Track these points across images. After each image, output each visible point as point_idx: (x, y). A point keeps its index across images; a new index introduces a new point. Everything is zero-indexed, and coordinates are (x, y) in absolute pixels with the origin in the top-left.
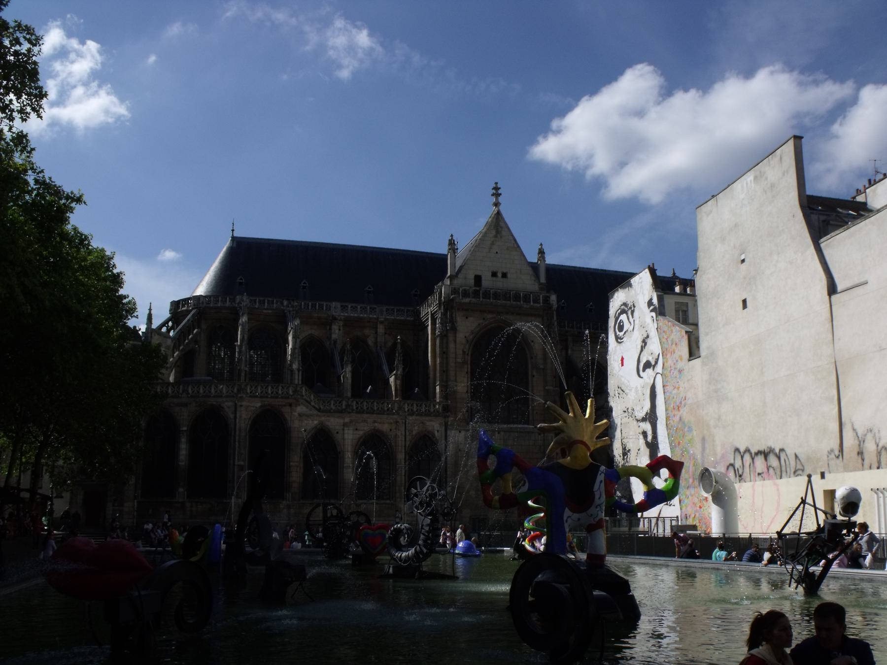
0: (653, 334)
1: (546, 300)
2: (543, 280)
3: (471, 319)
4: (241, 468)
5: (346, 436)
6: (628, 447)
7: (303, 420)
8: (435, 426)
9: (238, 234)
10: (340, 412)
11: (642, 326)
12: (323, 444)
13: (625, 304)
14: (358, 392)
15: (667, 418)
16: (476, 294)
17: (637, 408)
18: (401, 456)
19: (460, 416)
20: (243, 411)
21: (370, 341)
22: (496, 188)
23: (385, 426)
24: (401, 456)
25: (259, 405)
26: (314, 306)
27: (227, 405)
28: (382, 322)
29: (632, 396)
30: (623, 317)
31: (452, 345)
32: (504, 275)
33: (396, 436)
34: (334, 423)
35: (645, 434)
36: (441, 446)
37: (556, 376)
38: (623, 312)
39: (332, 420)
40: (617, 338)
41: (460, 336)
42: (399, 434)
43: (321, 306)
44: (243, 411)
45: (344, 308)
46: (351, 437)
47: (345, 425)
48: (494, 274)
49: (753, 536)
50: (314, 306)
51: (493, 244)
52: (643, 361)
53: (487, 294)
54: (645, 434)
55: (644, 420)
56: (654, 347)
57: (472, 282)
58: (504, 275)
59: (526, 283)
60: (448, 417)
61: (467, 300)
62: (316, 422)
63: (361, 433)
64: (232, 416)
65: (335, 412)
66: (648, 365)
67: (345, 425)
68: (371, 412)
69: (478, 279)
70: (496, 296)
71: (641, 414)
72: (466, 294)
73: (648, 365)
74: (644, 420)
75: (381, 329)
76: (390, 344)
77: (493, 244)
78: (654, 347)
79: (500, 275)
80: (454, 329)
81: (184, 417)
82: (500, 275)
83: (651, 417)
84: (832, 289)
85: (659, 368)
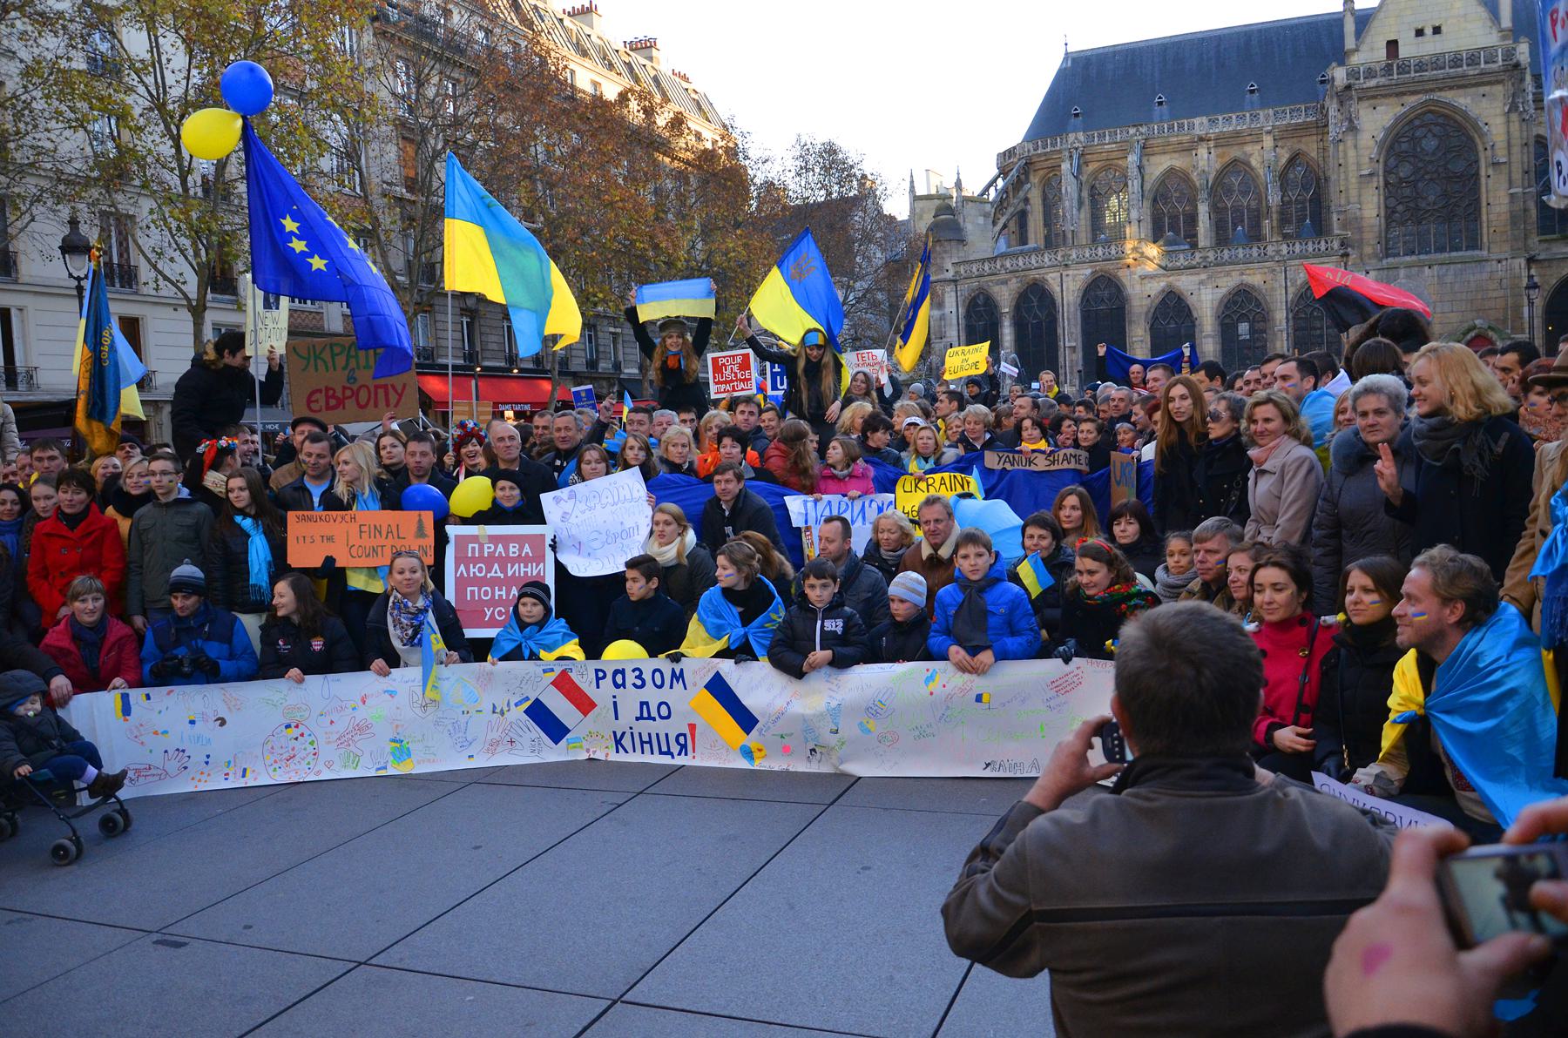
1: (1509, 54)
2: (1506, 22)
4: (1073, 349)
5: (1203, 297)
9: (1074, 47)
11: (1026, 200)
12: (1173, 314)
16: (1388, 69)
18: (1280, 316)
19: (1368, 250)
20: (1067, 287)
23: (1255, 278)
24: (1280, 316)
25: (1089, 271)
26: (1171, 128)
28: (1269, 132)
31: (1351, 153)
32: (1437, 30)
33: (1273, 289)
34: (1185, 283)
37: (164, 775)
39: (1183, 278)
42: (1276, 285)
43: (1181, 126)
44: (1067, 287)
45: (1213, 122)
46: (1210, 297)
47: (1201, 283)
48: (1420, 33)
50: (1171, 128)
53: (1404, 68)
57: (1382, 54)
58: (1437, 30)
61: (1373, 83)
62: (1163, 284)
63: (1224, 290)
64: (1058, 289)
65: (1186, 268)
68: (1233, 262)
69: (1392, 46)
70: (1421, 67)
72: (1370, 74)
75: (1268, 141)
79: (1428, 31)
80: (1353, 129)
81: (1005, 297)
82: (1428, 31)
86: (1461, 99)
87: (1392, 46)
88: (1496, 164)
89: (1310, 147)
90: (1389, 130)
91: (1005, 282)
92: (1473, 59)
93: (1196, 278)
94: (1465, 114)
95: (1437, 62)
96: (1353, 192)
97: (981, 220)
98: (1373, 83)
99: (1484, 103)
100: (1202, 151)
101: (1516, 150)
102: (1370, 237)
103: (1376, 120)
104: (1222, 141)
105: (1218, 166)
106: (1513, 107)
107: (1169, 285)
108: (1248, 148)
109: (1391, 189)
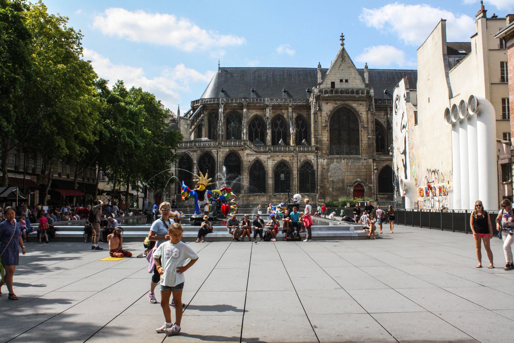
2: (367, 82)
7: (248, 157)
8: (311, 157)
10: (265, 152)
12: (258, 167)
19: (324, 152)
22: (342, 36)
31: (320, 118)
32: (347, 81)
36: (315, 168)
41: (324, 114)
43: (261, 100)
48: (341, 81)
51: (340, 65)
53: (337, 92)
54: (403, 160)
55: (403, 154)
61: (327, 95)
63: (276, 162)
64: (216, 156)
66: (404, 127)
69: (333, 84)
70: (342, 92)
72: (326, 92)
74: (403, 154)
75: (290, 110)
77: (340, 65)
79: (344, 81)
80: (320, 110)
82: (344, 81)
83: (404, 153)
86: (354, 105)
87: (333, 84)
88: (364, 127)
89: (304, 114)
90: (331, 112)
91: (195, 151)
92: (357, 92)
93: (266, 156)
94: (355, 109)
95: (347, 91)
96: (320, 131)
97: (186, 126)
98: (327, 95)
99: (361, 107)
100: (268, 110)
101: (370, 123)
102: (325, 147)
103: (328, 108)
104: (274, 108)
105: (273, 116)
106: (369, 110)
107: (257, 158)
108: (283, 111)
109: (332, 132)
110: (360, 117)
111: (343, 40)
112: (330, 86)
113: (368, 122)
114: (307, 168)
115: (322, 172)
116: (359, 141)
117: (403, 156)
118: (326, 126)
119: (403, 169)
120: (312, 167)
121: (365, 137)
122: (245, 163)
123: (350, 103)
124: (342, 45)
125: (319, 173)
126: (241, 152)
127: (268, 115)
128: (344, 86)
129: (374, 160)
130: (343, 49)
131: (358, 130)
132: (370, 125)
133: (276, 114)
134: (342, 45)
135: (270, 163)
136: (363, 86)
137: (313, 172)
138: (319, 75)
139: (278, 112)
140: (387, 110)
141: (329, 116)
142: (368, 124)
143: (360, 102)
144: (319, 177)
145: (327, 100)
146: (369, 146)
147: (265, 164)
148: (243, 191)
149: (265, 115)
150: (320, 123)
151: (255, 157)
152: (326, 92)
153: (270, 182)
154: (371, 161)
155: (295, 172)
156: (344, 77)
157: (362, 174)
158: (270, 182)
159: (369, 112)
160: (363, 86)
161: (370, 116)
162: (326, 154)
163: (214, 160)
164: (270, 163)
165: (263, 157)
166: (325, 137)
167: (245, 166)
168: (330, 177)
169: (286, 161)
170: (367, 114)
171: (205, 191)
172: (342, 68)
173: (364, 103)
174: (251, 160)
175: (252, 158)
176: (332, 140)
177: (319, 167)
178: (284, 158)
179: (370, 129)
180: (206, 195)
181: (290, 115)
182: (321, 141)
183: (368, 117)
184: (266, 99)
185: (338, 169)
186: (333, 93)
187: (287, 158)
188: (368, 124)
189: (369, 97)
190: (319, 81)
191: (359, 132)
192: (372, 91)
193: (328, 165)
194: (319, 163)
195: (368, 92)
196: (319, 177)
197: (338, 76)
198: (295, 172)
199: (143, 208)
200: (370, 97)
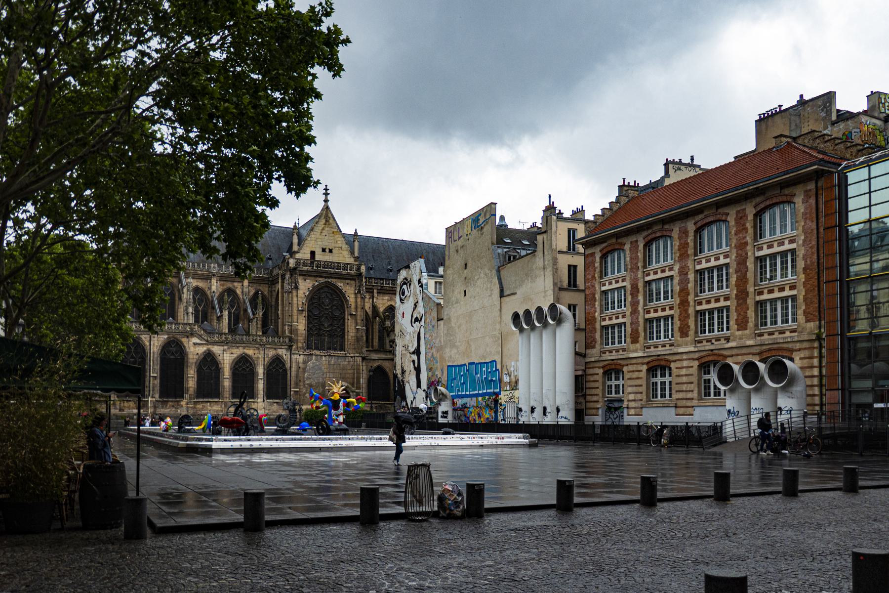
0: (420, 301)
3: (308, 281)
6: (405, 368)
7: (195, 348)
8: (283, 352)
12: (209, 362)
13: (406, 279)
14: (232, 330)
15: (426, 354)
17: (410, 345)
19: (300, 345)
21: (239, 291)
27: (145, 338)
29: (408, 337)
30: (405, 287)
31: (295, 299)
32: (331, 251)
35: (414, 362)
36: (288, 366)
38: (405, 283)
40: (401, 299)
41: (301, 293)
48: (324, 250)
49: (690, 424)
51: (323, 229)
52: (415, 317)
54: (414, 362)
55: (413, 353)
56: (421, 309)
59: (343, 256)
60: (193, 252)
63: (235, 356)
64: (148, 344)
66: (417, 320)
67: (224, 350)
69: (313, 253)
71: (412, 350)
73: (417, 320)
74: (413, 353)
76: (252, 293)
78: (421, 309)
79: (327, 250)
80: (297, 288)
83: (417, 352)
84: (502, 295)
85: (422, 323)
86: (340, 284)
87: (313, 253)
88: (351, 315)
94: (340, 290)
95: (328, 265)
96: (295, 317)
99: (348, 287)
100: (214, 281)
101: (359, 310)
103: (305, 286)
105: (221, 290)
106: (359, 292)
107: (209, 350)
108: (236, 284)
109: (310, 319)
110: (347, 301)
111: (326, 194)
112: (308, 256)
113: (356, 308)
114: (244, 364)
115: (297, 371)
116: (344, 333)
117: (415, 357)
118: (303, 310)
119: (414, 372)
120: (284, 365)
121: (353, 327)
122: (190, 356)
123: (334, 281)
124: (326, 201)
125: (293, 374)
126: (184, 340)
127: (214, 288)
128: (327, 258)
129: (364, 359)
130: (327, 209)
131: (344, 318)
132: (359, 313)
133: (225, 287)
134: (326, 201)
135: (227, 358)
136: (351, 260)
137: (285, 371)
138: (295, 240)
139: (229, 285)
140: (373, 292)
141: (307, 297)
142: (356, 311)
143: (347, 281)
144: (293, 379)
145: (305, 275)
146: (358, 340)
147: (220, 358)
148: (187, 396)
149: (210, 288)
150: (295, 306)
151: (205, 348)
152: (304, 265)
153: (227, 383)
154: (359, 359)
155: (261, 370)
156: (328, 245)
157: (348, 376)
158: (227, 383)
159: (359, 295)
160: (351, 260)
161: (359, 300)
162: (303, 348)
163: (144, 350)
164: (227, 358)
165: (216, 349)
166: (301, 325)
167: (190, 360)
168: (308, 378)
169: (249, 356)
170: (356, 298)
171: (339, 400)
172: (325, 232)
173: (353, 282)
174: (200, 353)
175: (202, 350)
176: (309, 330)
177: (294, 365)
178: (247, 351)
179: (359, 317)
180: (341, 404)
181: (246, 290)
182: (297, 330)
183: (356, 302)
184: (212, 265)
185: (310, 367)
186: (314, 268)
187: (250, 352)
188: (356, 311)
189: (360, 275)
190: (295, 248)
191: (344, 321)
192: (363, 268)
193: (305, 362)
194: (295, 359)
195: (359, 268)
196: (293, 379)
197: (320, 243)
198: (261, 370)
199: (579, 413)
200: (361, 274)
